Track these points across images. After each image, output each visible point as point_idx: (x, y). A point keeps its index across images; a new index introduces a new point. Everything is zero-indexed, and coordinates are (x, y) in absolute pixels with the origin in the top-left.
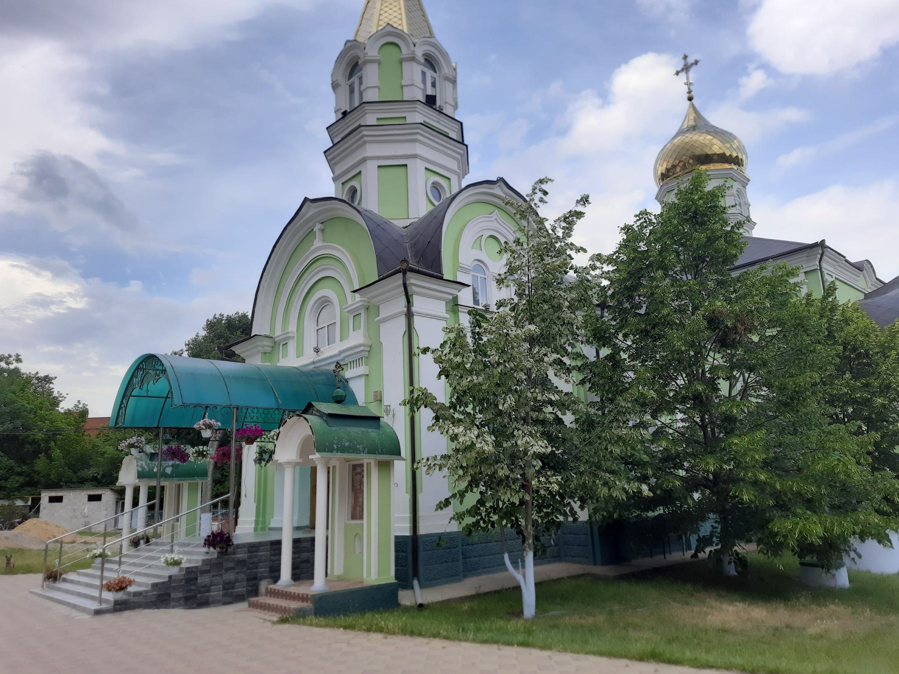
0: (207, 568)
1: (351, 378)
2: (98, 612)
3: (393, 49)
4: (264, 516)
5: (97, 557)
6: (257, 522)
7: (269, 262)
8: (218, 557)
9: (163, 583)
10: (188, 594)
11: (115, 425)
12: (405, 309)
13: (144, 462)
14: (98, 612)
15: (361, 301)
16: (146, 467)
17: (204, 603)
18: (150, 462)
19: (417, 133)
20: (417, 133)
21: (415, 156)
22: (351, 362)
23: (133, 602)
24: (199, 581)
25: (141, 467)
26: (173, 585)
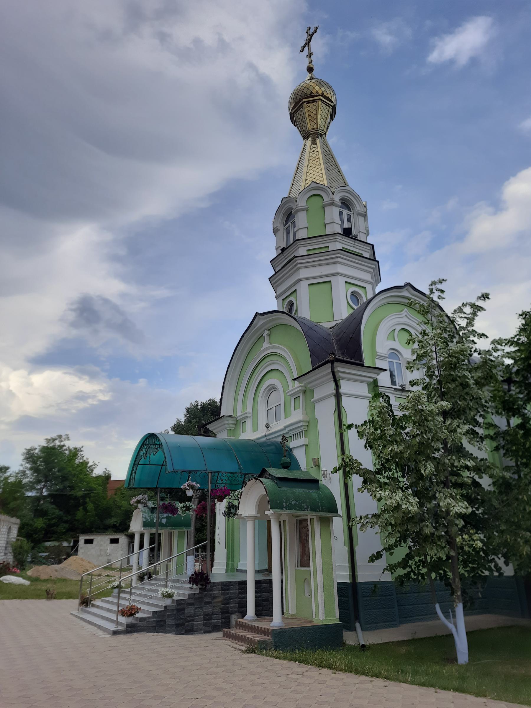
0: (192, 601)
1: (294, 448)
2: (115, 633)
3: (317, 199)
4: (233, 560)
5: (115, 588)
6: (227, 564)
7: (232, 361)
8: (200, 593)
9: (161, 611)
10: (179, 622)
11: (128, 486)
12: (334, 392)
13: (147, 515)
14: (115, 633)
15: (300, 387)
16: (148, 518)
17: (190, 631)
18: (151, 514)
21: (337, 274)
22: (293, 435)
23: (140, 626)
24: (186, 612)
25: (145, 518)
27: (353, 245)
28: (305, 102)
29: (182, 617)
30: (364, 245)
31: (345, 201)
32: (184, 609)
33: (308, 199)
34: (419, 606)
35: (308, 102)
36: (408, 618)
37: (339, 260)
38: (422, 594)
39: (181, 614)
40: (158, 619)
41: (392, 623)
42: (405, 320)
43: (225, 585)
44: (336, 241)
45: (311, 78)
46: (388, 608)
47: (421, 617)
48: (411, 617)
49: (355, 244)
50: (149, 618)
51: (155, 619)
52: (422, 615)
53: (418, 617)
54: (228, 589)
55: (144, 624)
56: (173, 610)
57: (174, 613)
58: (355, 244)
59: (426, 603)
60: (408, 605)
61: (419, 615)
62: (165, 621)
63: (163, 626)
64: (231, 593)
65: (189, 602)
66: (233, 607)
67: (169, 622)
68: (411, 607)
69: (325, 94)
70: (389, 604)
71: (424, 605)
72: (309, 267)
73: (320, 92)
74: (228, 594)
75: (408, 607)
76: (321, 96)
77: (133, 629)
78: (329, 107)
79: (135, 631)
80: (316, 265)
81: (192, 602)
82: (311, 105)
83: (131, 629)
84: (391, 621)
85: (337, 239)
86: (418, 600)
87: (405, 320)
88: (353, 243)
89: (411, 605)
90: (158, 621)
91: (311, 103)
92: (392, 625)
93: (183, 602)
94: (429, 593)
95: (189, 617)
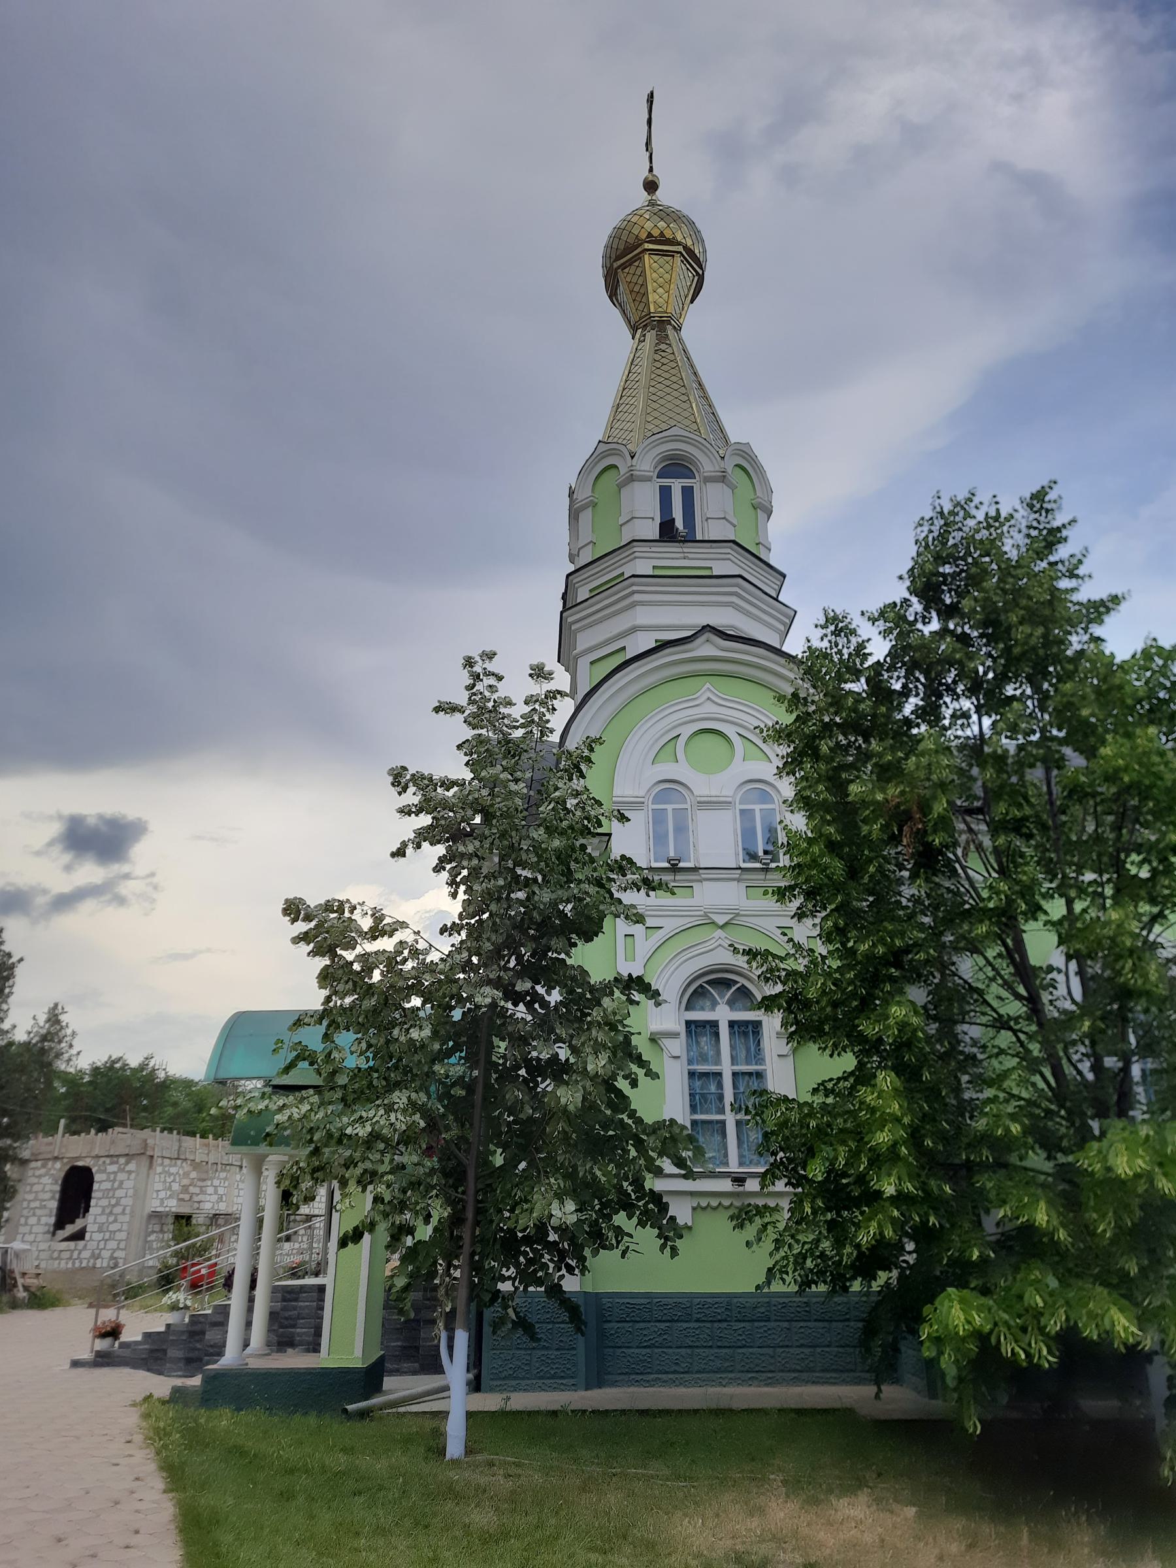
10: (191, 1355)
19: (634, 592)
20: (634, 592)
21: (634, 629)
23: (118, 1356)
24: (207, 1337)
26: (171, 1338)
27: (682, 555)
28: (619, 267)
29: (198, 1346)
30: (711, 548)
31: (677, 459)
32: (203, 1333)
33: (594, 484)
34: (670, 1351)
35: (623, 267)
36: (633, 1377)
37: (637, 597)
38: (679, 1324)
39: (198, 1341)
40: (152, 1347)
41: (564, 1382)
42: (710, 708)
43: (289, 1292)
44: (635, 558)
45: (652, 203)
46: (557, 1349)
47: (671, 1376)
48: (642, 1374)
49: (685, 550)
50: (136, 1343)
51: (146, 1347)
52: (675, 1372)
53: (660, 1376)
54: (296, 1300)
55: (126, 1353)
56: (183, 1332)
57: (184, 1338)
58: (685, 550)
59: (690, 1347)
60: (637, 1347)
61: (667, 1373)
62: (165, 1351)
63: (161, 1359)
64: (301, 1307)
65: (214, 1320)
66: (304, 1333)
67: (174, 1353)
68: (644, 1351)
69: (656, 233)
70: (561, 1341)
71: (683, 1351)
72: (590, 626)
73: (643, 236)
74: (295, 1308)
75: (637, 1351)
76: (647, 242)
77: (106, 1360)
78: (673, 256)
79: (108, 1365)
80: (601, 618)
81: (220, 1320)
82: (662, 260)
83: (103, 1360)
84: (562, 1378)
85: (637, 554)
86: (665, 1337)
87: (710, 708)
88: (680, 550)
89: (645, 1347)
90: (152, 1351)
91: (630, 265)
92: (562, 1387)
93: (202, 1320)
94: (702, 1325)
95: (211, 1346)
